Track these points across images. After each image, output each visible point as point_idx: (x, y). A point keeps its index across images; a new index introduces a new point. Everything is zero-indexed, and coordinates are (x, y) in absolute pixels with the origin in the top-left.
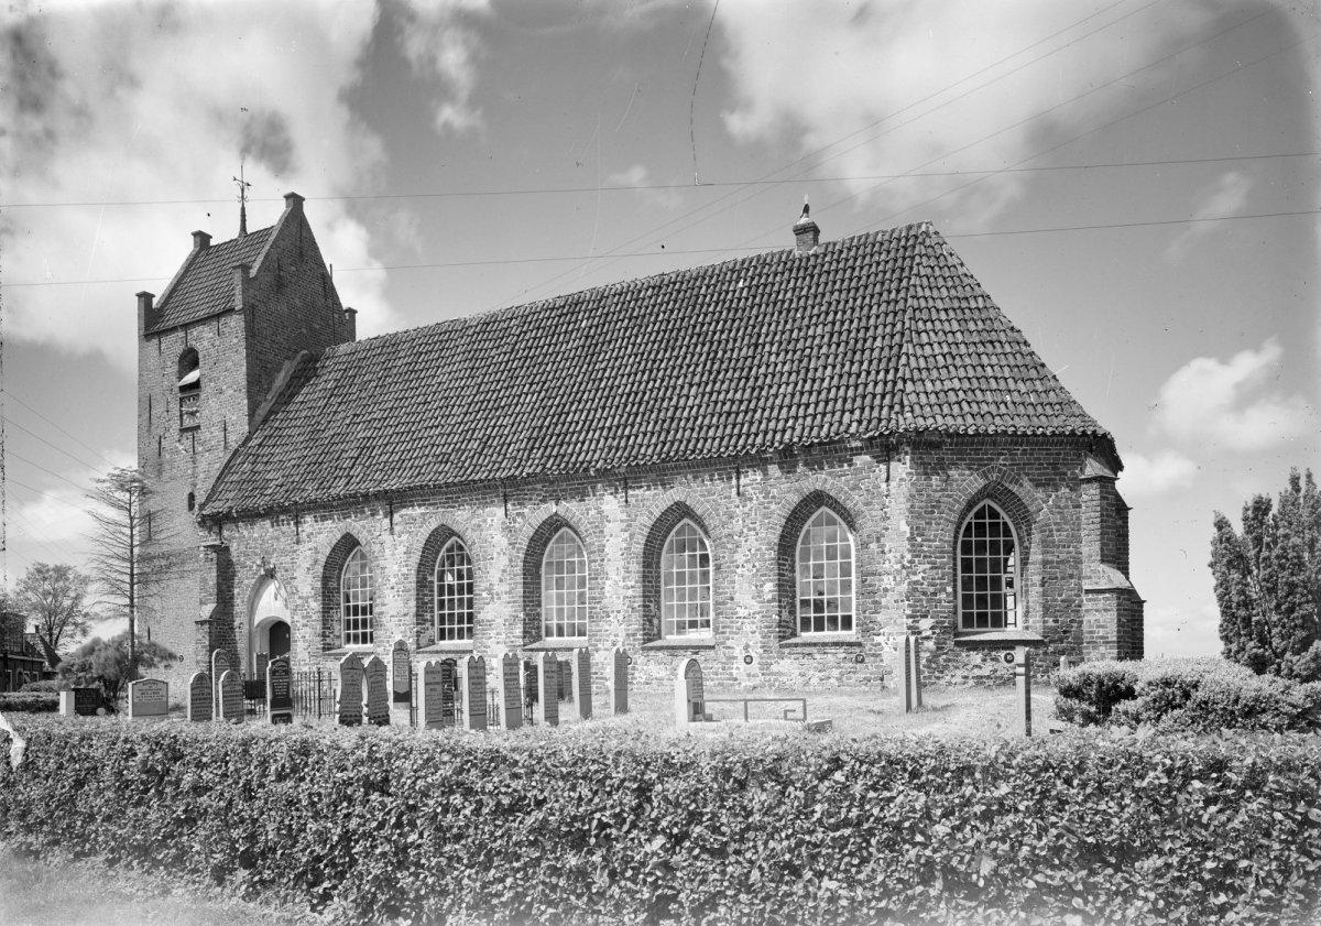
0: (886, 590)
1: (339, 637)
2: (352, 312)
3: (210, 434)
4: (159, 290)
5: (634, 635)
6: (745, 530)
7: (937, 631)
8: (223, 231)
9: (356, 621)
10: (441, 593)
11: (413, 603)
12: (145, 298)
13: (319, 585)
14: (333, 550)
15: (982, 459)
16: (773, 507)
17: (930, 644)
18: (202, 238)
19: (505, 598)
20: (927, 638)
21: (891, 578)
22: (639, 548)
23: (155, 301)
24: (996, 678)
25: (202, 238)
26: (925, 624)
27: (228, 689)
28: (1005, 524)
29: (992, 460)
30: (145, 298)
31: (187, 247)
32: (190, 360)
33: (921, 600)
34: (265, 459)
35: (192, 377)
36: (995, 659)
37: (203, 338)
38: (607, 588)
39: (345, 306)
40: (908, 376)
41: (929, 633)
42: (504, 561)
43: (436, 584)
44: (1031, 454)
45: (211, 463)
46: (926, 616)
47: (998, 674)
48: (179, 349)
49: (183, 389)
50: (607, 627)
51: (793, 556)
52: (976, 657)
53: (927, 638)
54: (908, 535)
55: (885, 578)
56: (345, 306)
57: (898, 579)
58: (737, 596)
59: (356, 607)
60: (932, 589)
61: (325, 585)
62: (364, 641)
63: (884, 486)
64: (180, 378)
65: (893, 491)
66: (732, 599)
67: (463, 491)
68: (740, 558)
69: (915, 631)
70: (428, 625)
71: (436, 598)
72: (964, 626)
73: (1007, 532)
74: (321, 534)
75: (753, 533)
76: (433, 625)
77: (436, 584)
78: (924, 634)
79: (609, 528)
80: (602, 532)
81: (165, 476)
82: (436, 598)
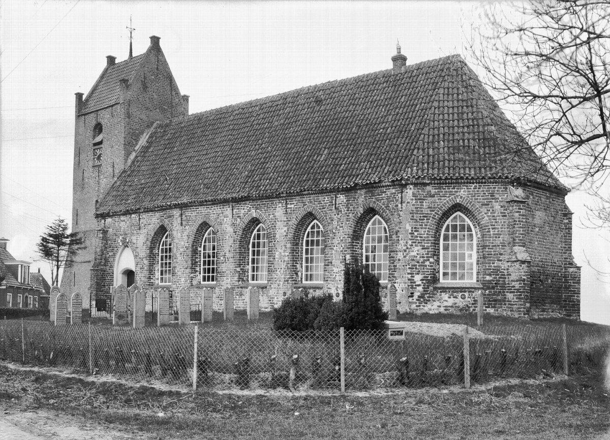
0: (399, 260)
1: (158, 279)
2: (186, 98)
3: (107, 169)
4: (86, 92)
5: (288, 281)
6: (338, 227)
7: (425, 282)
8: (121, 57)
9: (209, 261)
10: (204, 257)
11: (190, 262)
12: (79, 96)
13: (148, 251)
14: (155, 233)
15: (451, 192)
16: (351, 215)
17: (420, 289)
18: (111, 60)
19: (231, 260)
20: (419, 285)
21: (402, 253)
22: (290, 236)
23: (84, 97)
24: (456, 307)
25: (111, 60)
26: (418, 278)
27: (75, 301)
28: (469, 225)
29: (457, 192)
30: (79, 96)
31: (104, 64)
32: (98, 128)
33: (416, 265)
34: (130, 184)
35: (98, 139)
36: (456, 297)
37: (105, 118)
38: (277, 256)
39: (182, 93)
40: (421, 146)
41: (420, 283)
42: (231, 241)
43: (202, 252)
44: (479, 188)
45: (106, 182)
46: (418, 274)
47: (457, 305)
48: (94, 123)
49: (95, 144)
50: (276, 276)
51: (362, 241)
52: (445, 296)
53: (419, 285)
54: (410, 231)
55: (399, 253)
56: (182, 93)
57: (405, 254)
58: (333, 261)
59: (312, 241)
60: (422, 260)
61: (151, 252)
62: (213, 280)
63: (400, 205)
64: (94, 137)
65: (404, 208)
66: (331, 263)
67: (213, 204)
68: (336, 241)
69: (412, 281)
70: (198, 273)
71: (202, 259)
72: (443, 279)
73: (469, 230)
74: (152, 221)
75: (341, 229)
76: (200, 273)
77: (202, 252)
78: (417, 284)
79: (279, 224)
80: (275, 226)
81: (86, 190)
82: (202, 259)
